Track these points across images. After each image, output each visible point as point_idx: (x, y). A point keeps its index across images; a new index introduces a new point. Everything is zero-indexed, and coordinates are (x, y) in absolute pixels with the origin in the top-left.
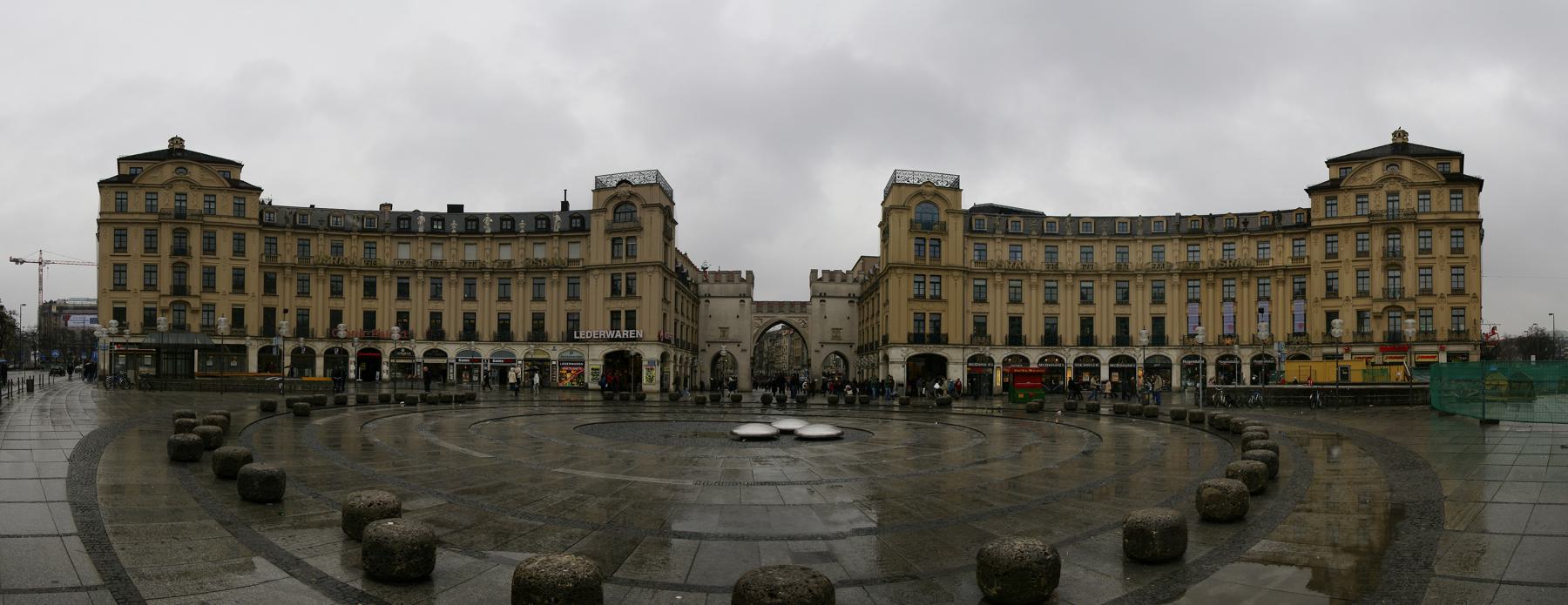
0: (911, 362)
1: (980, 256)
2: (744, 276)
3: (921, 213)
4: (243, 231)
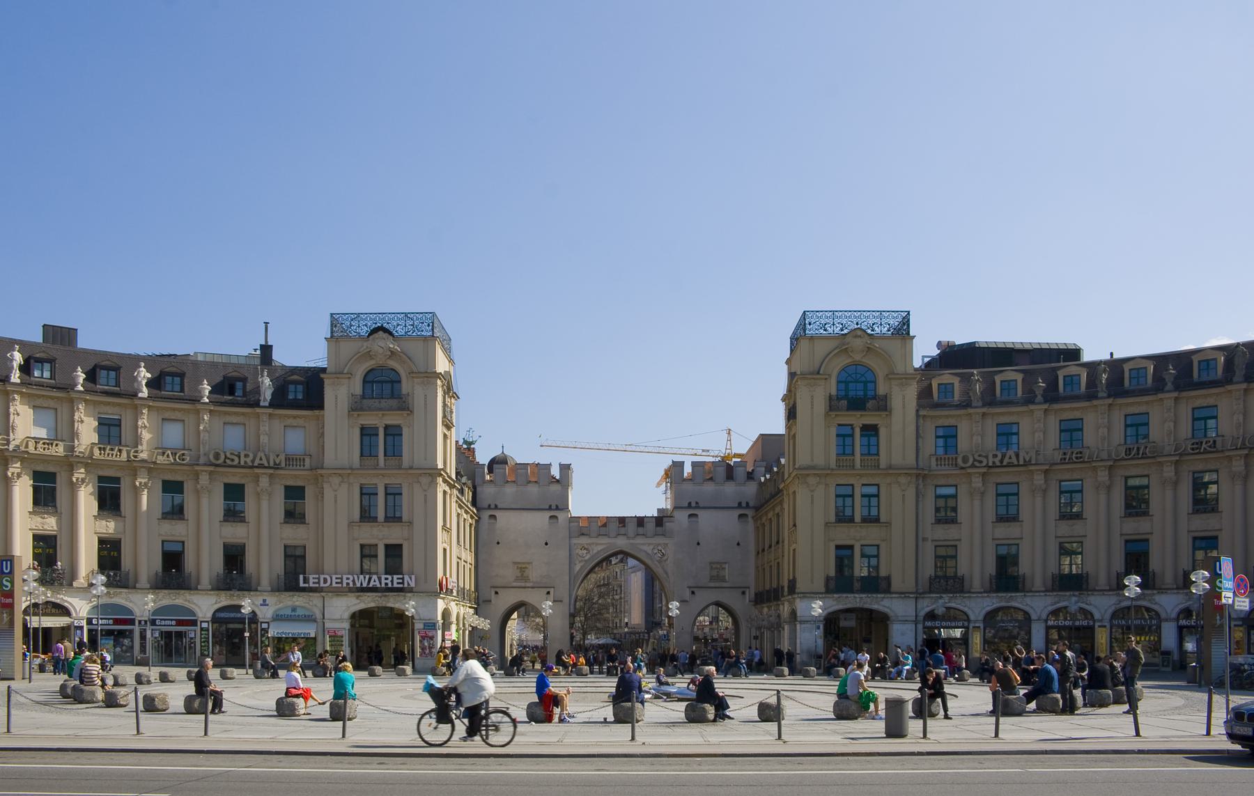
0: (831, 623)
2: (555, 472)
3: (846, 383)
4: (712, 585)
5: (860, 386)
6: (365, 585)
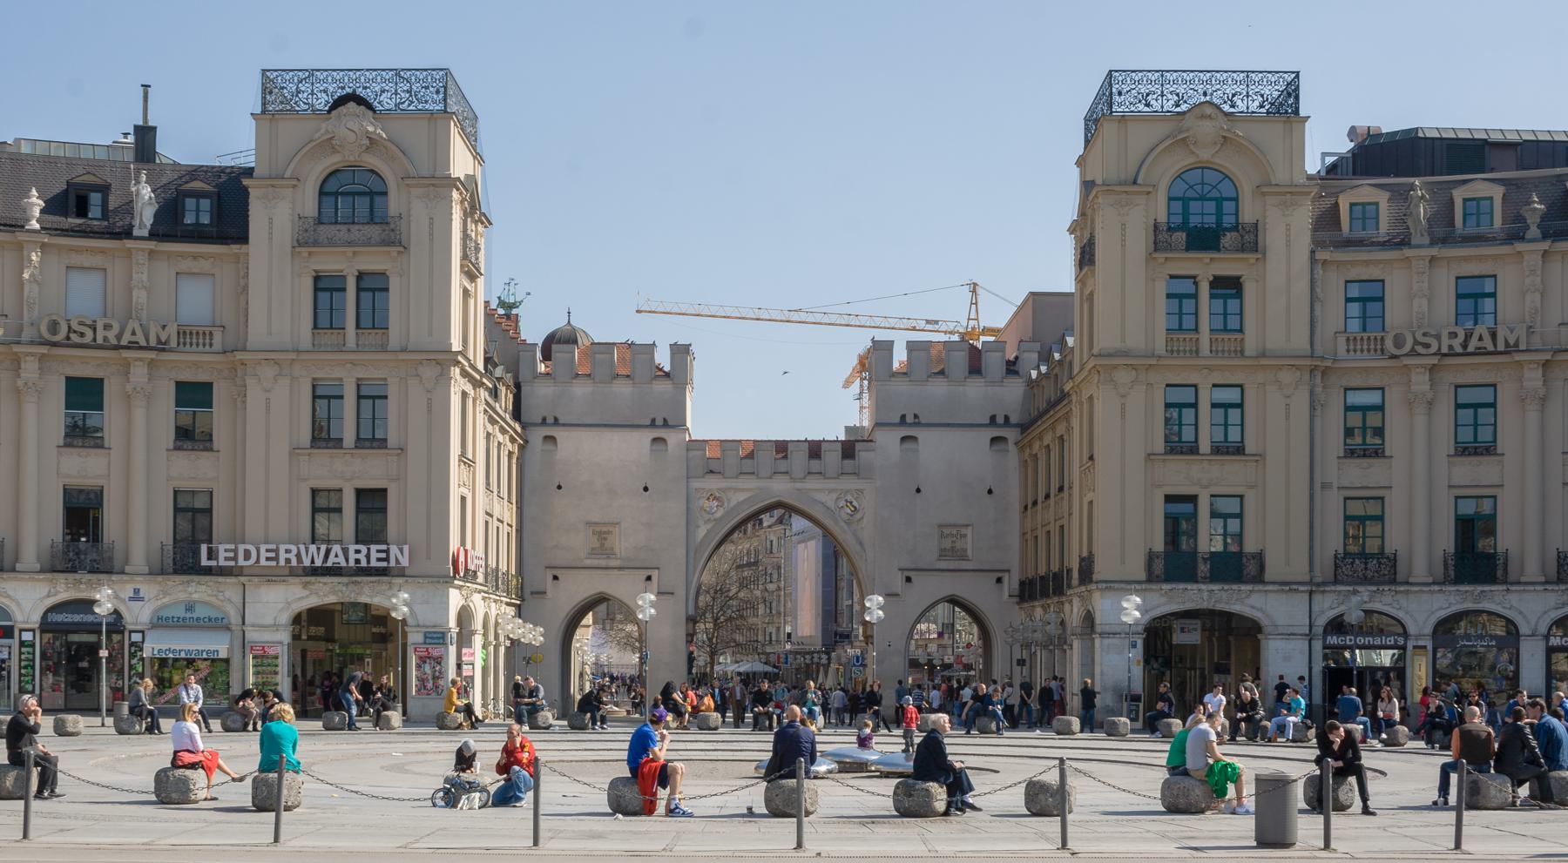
1: (1364, 317)
2: (663, 359)
4: (943, 565)
5: (1210, 207)
6: (318, 563)
